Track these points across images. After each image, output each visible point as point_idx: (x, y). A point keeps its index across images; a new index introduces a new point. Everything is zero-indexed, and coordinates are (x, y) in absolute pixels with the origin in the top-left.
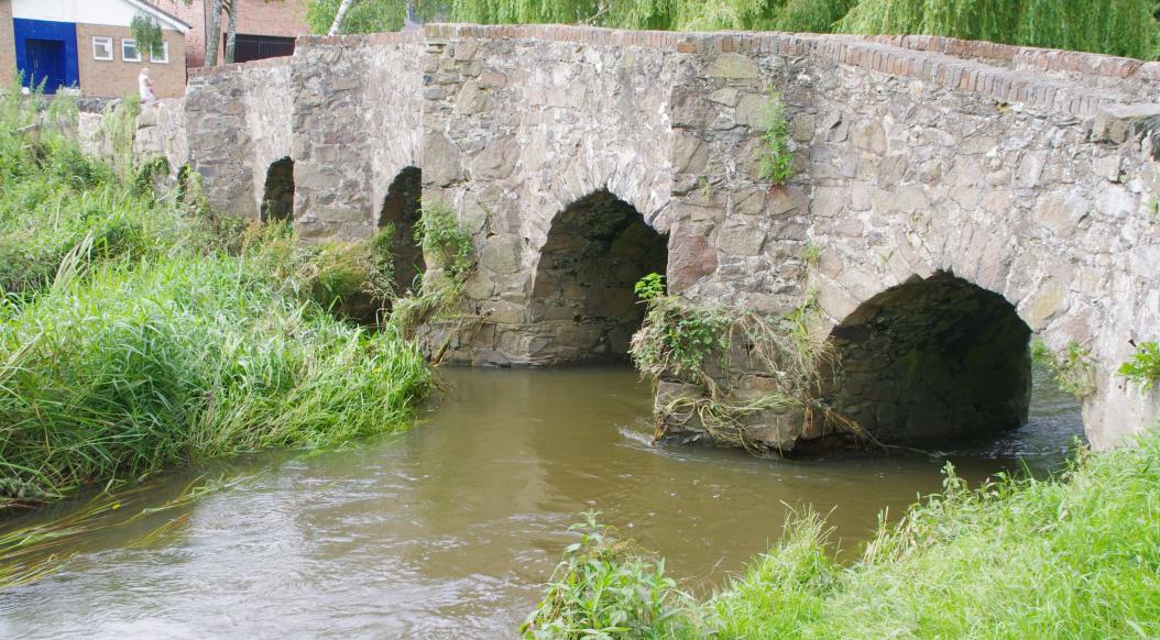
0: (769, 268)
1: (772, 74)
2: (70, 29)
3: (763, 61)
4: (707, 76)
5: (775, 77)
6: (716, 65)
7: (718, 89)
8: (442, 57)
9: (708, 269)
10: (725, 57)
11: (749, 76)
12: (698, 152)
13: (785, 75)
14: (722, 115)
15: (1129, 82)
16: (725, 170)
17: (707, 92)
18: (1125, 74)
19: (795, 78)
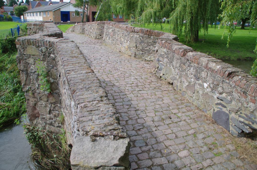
0: (53, 119)
1: (43, 54)
2: (69, 12)
3: (40, 49)
4: (25, 54)
5: (44, 55)
6: (27, 50)
7: (28, 58)
8: (31, 31)
9: (38, 116)
10: (29, 47)
11: (37, 54)
12: (27, 79)
13: (47, 54)
14: (31, 67)
15: (183, 59)
16: (35, 86)
17: (26, 59)
18: (182, 55)
19: (50, 56)
